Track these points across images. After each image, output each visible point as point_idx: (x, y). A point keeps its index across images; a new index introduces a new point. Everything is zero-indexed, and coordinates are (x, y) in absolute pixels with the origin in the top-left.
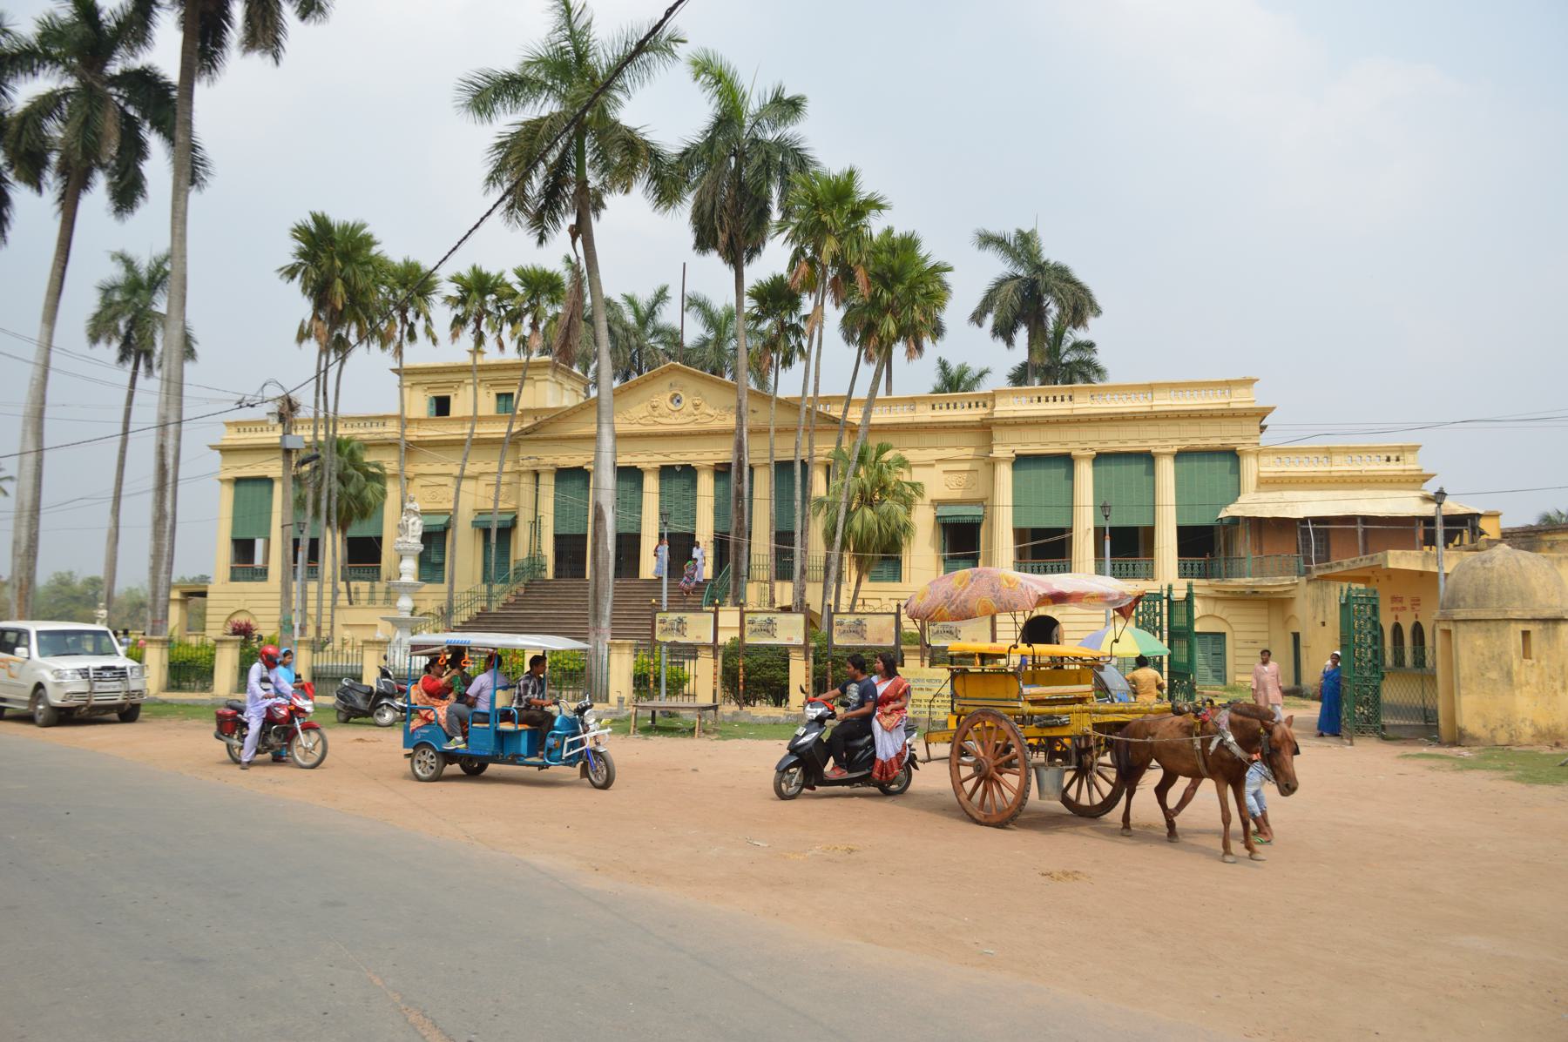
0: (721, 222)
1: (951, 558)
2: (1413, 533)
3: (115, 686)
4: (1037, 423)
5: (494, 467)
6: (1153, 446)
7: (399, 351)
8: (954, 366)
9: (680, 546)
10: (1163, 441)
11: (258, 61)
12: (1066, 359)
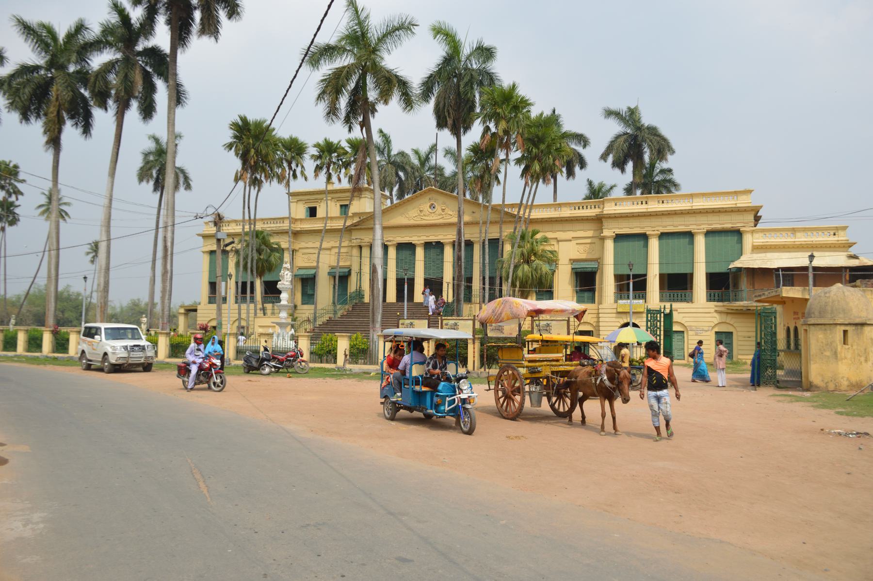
0: (449, 114)
1: (581, 291)
2: (841, 276)
3: (140, 354)
4: (627, 217)
5: (317, 245)
6: (692, 228)
7: (288, 185)
8: (596, 184)
9: (434, 285)
10: (699, 226)
11: (207, 41)
12: (657, 178)
